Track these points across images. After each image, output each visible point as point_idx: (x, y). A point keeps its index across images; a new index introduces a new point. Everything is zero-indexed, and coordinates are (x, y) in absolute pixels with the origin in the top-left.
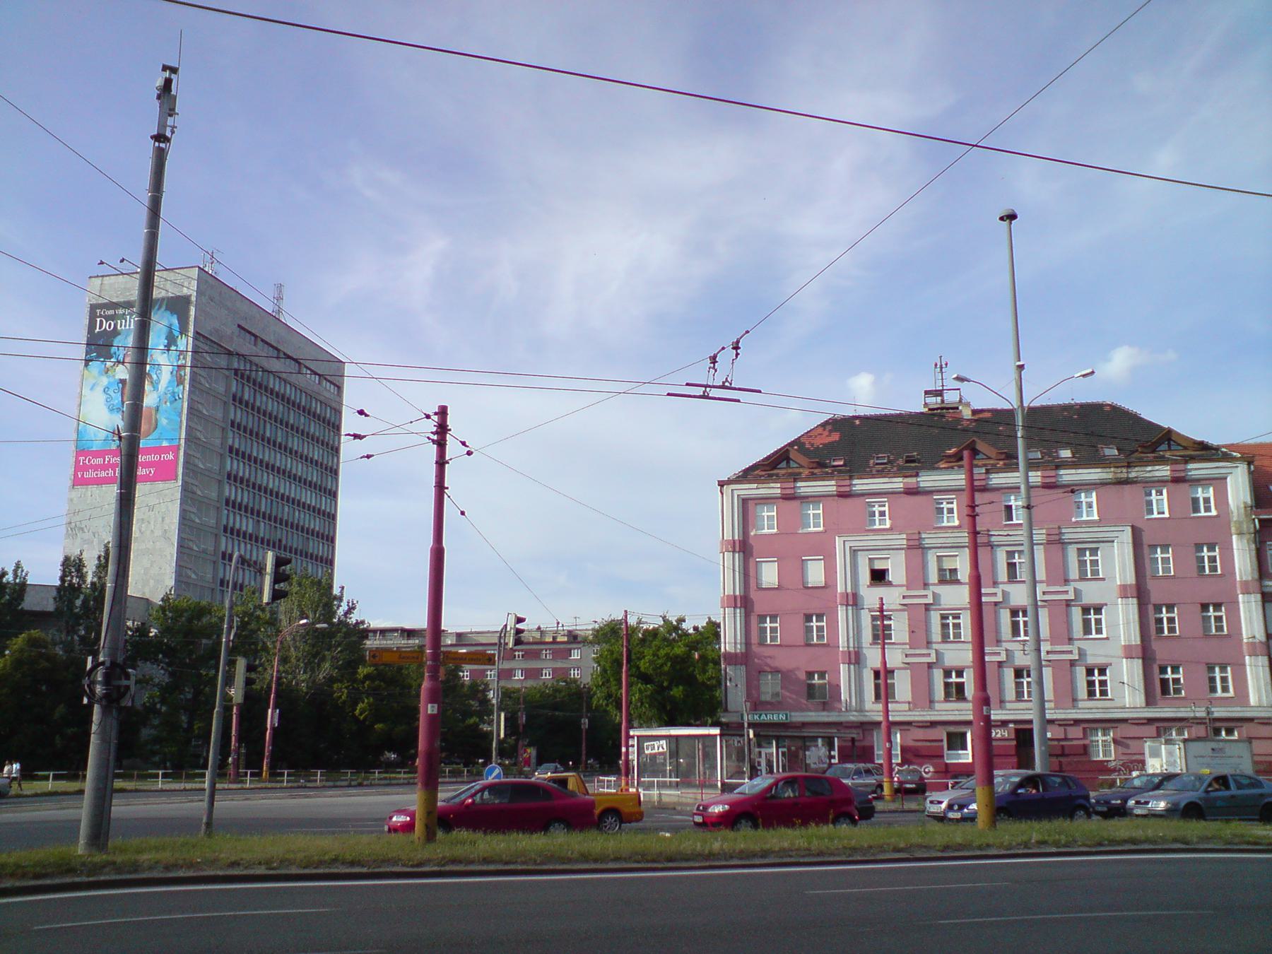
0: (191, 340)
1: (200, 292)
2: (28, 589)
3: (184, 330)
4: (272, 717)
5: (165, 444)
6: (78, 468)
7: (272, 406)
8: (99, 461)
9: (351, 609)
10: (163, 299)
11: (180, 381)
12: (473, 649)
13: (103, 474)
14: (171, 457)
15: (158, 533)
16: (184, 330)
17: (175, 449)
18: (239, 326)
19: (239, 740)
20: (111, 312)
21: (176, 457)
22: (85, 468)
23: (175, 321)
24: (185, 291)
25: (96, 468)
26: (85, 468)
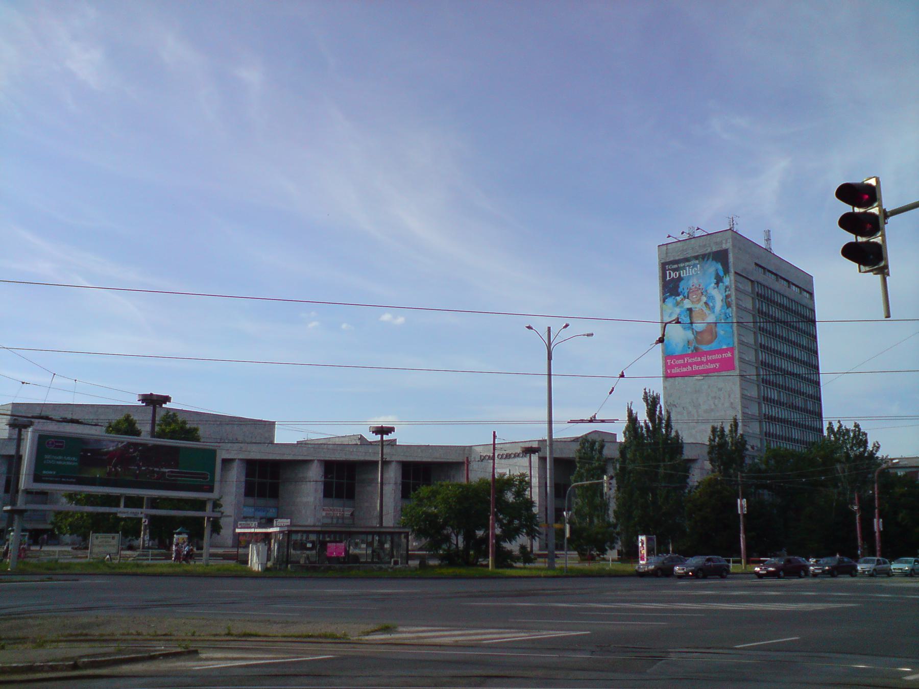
0: (732, 278)
1: (734, 246)
2: (685, 446)
3: (726, 271)
4: (878, 524)
5: (724, 347)
6: (667, 367)
7: (778, 314)
8: (680, 362)
9: (878, 448)
10: (709, 254)
11: (729, 305)
12: (908, 470)
13: (685, 370)
14: (729, 355)
15: (727, 404)
16: (726, 271)
17: (731, 350)
18: (756, 264)
19: (863, 539)
20: (675, 266)
21: (732, 354)
22: (672, 367)
23: (720, 266)
24: (724, 246)
25: (679, 366)
26: (672, 367)
